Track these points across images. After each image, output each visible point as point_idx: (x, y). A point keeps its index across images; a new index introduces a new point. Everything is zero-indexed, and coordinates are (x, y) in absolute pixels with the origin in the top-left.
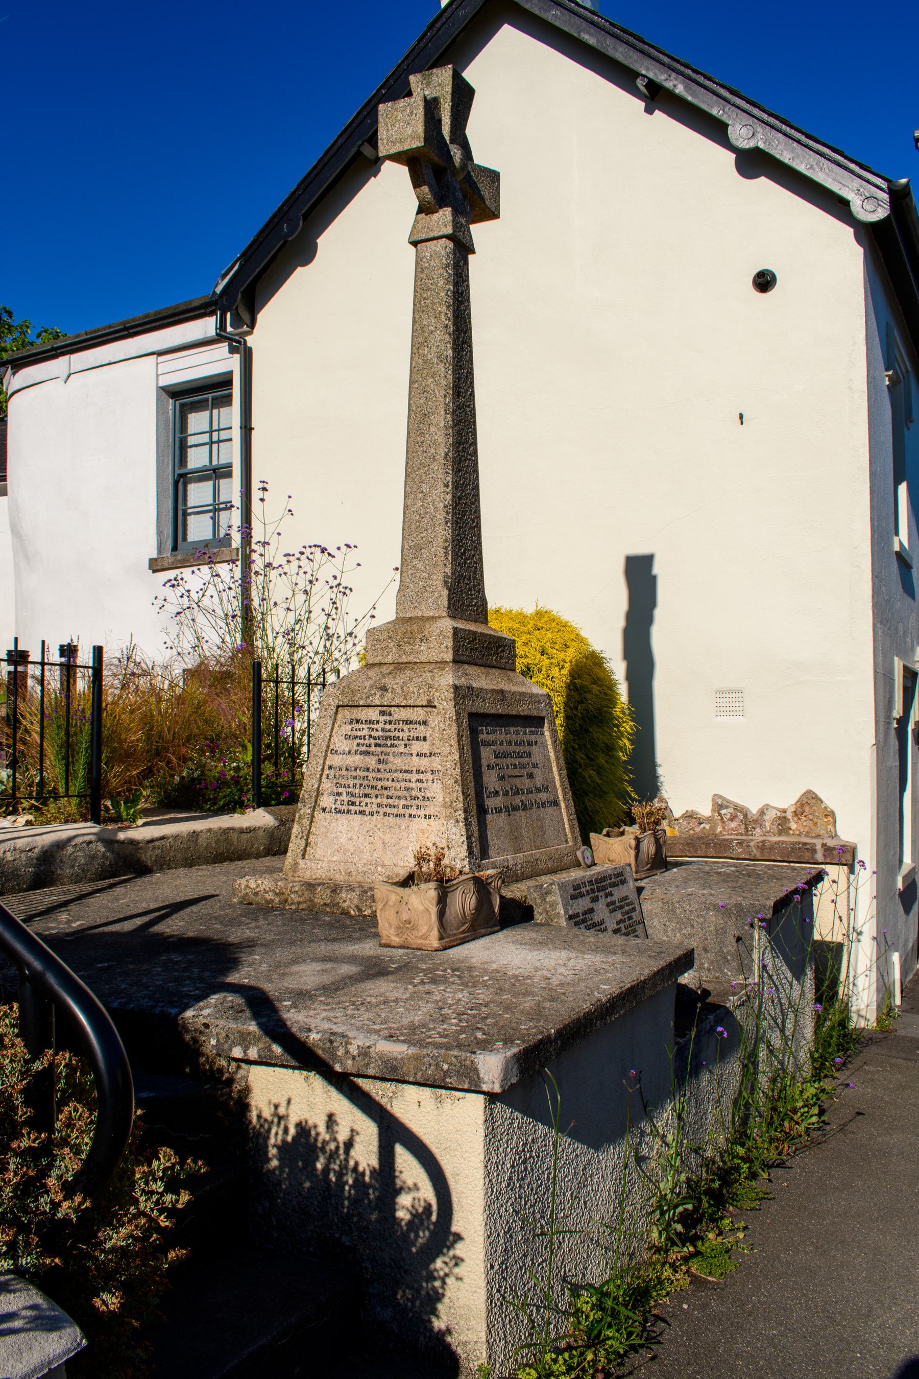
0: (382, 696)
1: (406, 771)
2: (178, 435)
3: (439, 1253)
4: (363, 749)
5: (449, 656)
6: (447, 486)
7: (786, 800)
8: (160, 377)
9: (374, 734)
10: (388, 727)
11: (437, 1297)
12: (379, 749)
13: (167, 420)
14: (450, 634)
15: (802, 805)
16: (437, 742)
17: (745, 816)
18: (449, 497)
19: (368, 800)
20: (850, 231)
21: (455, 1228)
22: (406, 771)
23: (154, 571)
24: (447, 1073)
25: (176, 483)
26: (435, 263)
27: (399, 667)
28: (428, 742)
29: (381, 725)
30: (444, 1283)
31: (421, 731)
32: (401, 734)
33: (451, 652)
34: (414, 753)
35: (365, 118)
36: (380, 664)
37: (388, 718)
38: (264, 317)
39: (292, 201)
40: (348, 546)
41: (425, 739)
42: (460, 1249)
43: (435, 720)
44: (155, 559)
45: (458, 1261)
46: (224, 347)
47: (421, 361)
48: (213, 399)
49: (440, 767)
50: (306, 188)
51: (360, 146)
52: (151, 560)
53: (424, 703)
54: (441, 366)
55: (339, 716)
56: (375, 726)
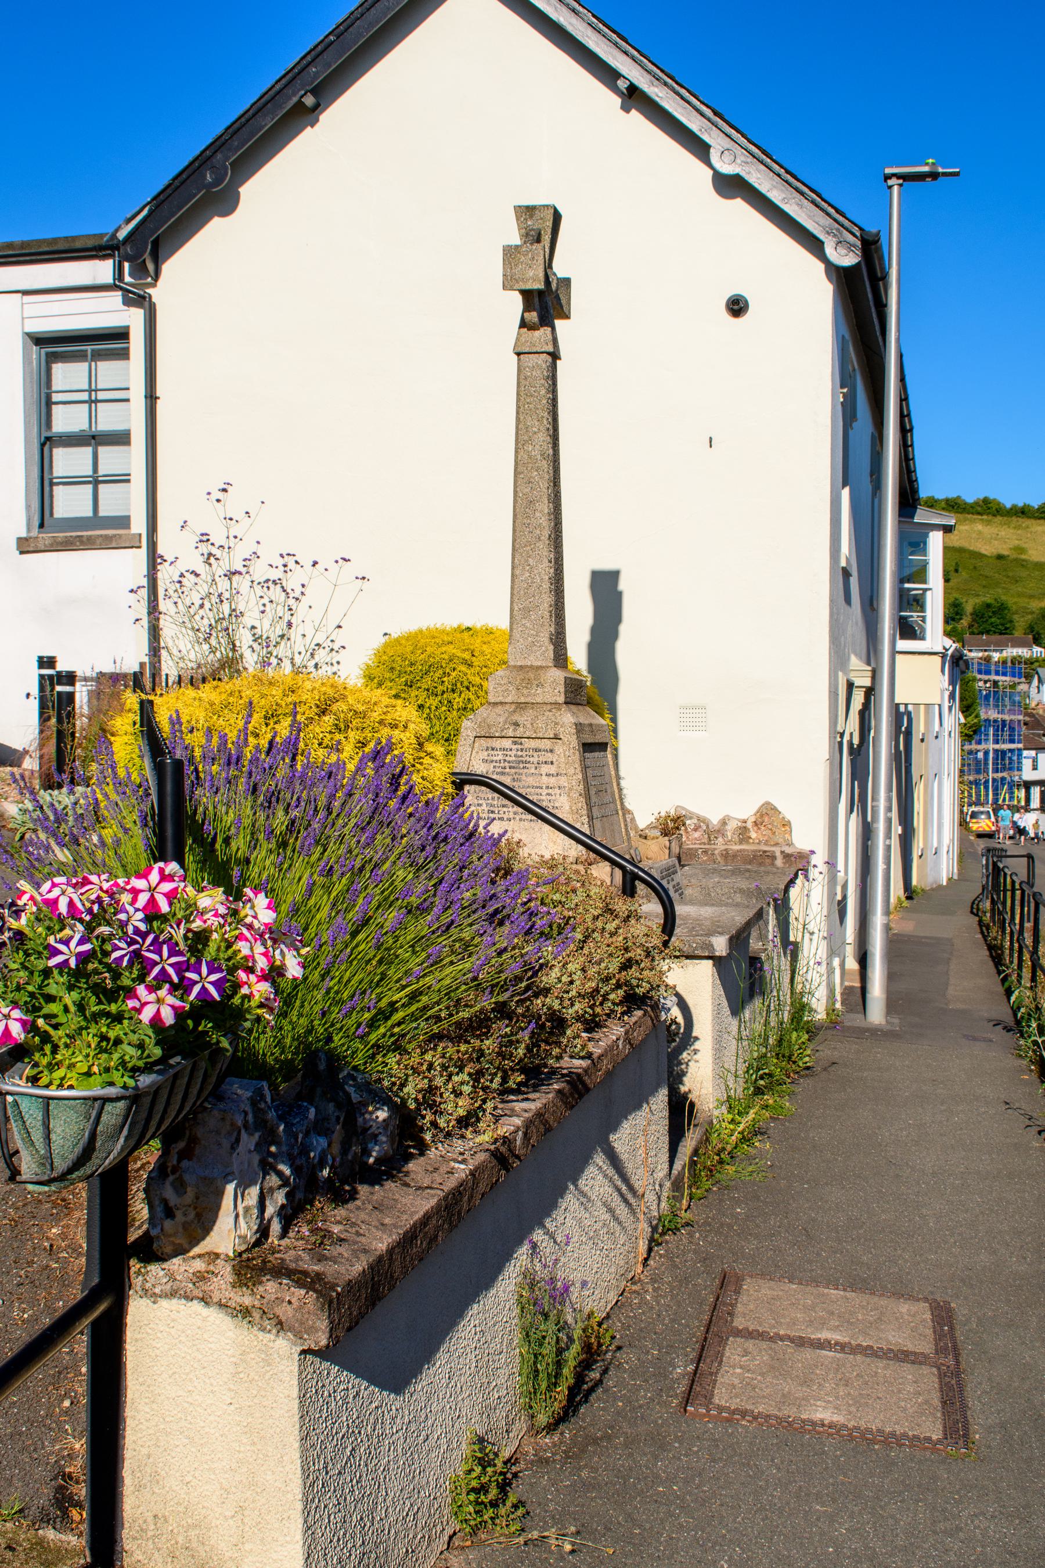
0: (515, 730)
1: (537, 787)
2: (44, 390)
3: (685, 1049)
4: (499, 770)
5: (561, 699)
6: (550, 562)
7: (745, 811)
8: (26, 321)
9: (508, 758)
10: (519, 753)
11: (683, 1074)
12: (513, 771)
13: (32, 372)
14: (562, 682)
15: (762, 816)
16: (563, 766)
17: (708, 826)
18: (552, 570)
19: (505, 809)
20: (821, 266)
21: (694, 1034)
22: (537, 787)
23: (22, 553)
24: (696, 948)
25: (43, 445)
26: (537, 373)
27: (521, 706)
28: (555, 765)
29: (514, 753)
30: (687, 1065)
31: (549, 757)
32: (531, 759)
33: (563, 695)
34: (544, 773)
35: (309, 64)
36: (501, 703)
37: (519, 747)
38: (168, 268)
39: (218, 145)
40: (344, 559)
41: (552, 763)
42: (697, 1045)
43: (559, 749)
44: (26, 539)
45: (696, 1052)
46: (117, 297)
47: (526, 456)
48: (93, 350)
49: (566, 784)
50: (235, 133)
51: (302, 97)
52: (19, 540)
53: (552, 736)
54: (544, 462)
55: (476, 745)
56: (509, 753)
